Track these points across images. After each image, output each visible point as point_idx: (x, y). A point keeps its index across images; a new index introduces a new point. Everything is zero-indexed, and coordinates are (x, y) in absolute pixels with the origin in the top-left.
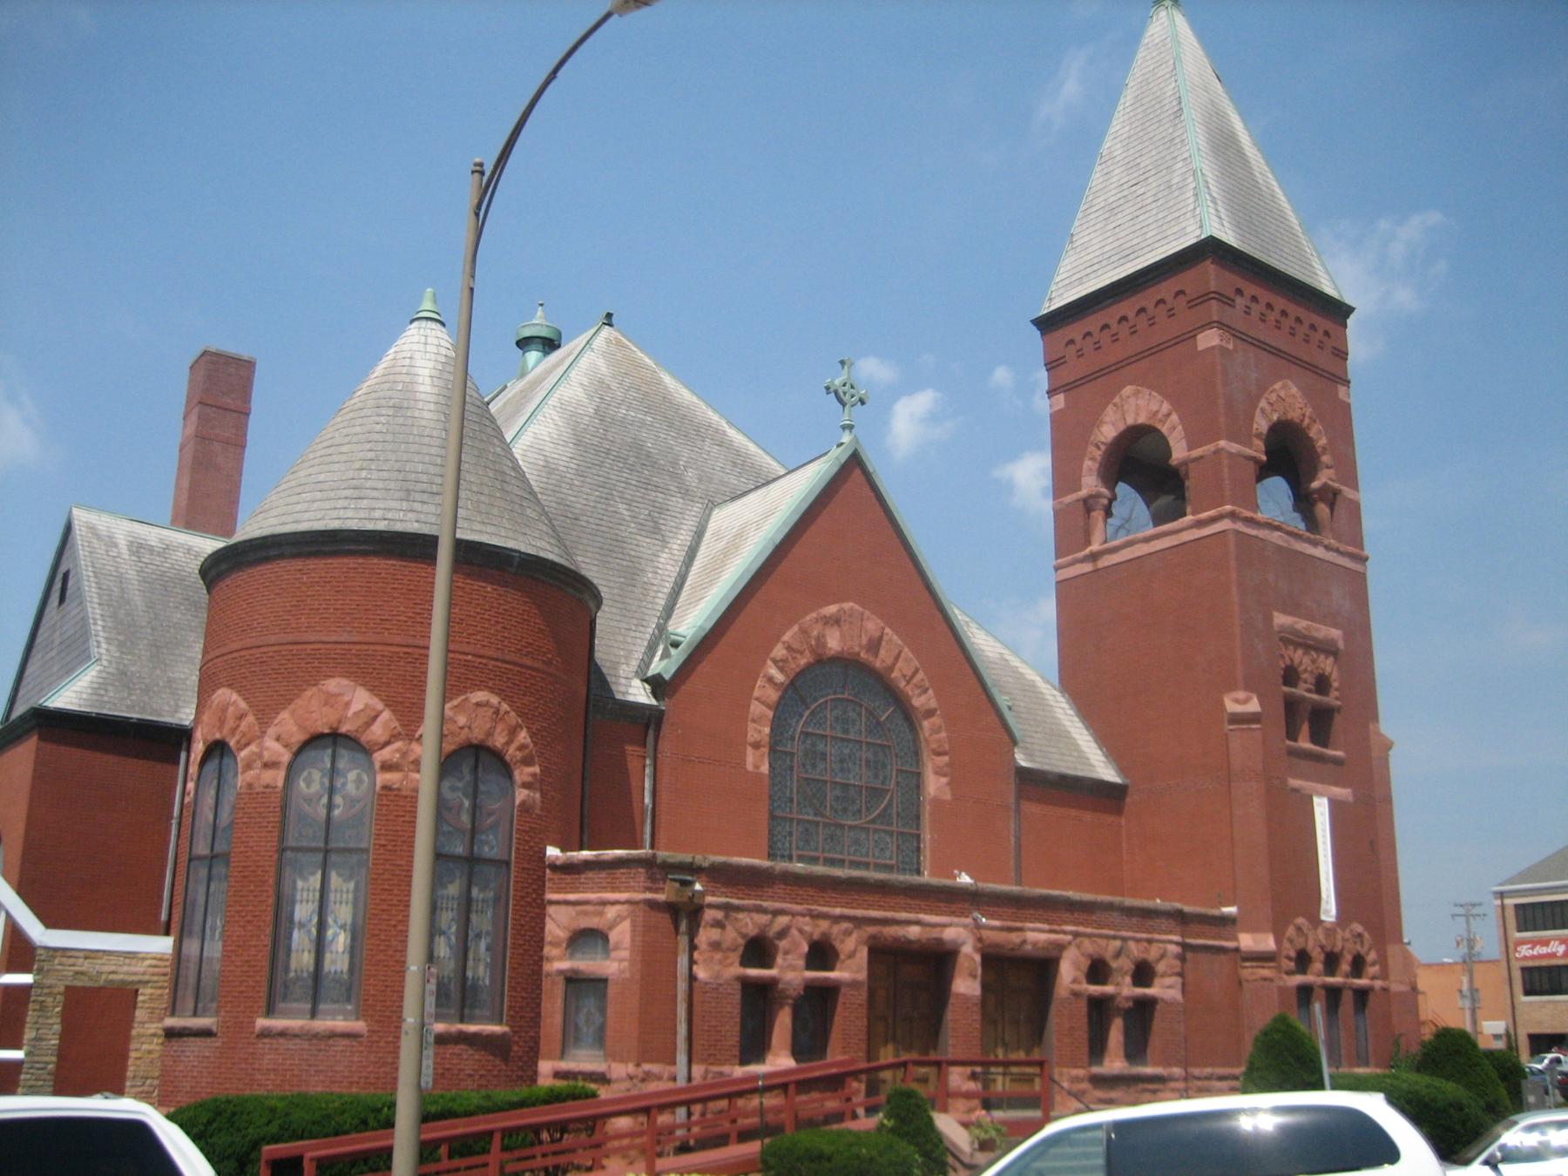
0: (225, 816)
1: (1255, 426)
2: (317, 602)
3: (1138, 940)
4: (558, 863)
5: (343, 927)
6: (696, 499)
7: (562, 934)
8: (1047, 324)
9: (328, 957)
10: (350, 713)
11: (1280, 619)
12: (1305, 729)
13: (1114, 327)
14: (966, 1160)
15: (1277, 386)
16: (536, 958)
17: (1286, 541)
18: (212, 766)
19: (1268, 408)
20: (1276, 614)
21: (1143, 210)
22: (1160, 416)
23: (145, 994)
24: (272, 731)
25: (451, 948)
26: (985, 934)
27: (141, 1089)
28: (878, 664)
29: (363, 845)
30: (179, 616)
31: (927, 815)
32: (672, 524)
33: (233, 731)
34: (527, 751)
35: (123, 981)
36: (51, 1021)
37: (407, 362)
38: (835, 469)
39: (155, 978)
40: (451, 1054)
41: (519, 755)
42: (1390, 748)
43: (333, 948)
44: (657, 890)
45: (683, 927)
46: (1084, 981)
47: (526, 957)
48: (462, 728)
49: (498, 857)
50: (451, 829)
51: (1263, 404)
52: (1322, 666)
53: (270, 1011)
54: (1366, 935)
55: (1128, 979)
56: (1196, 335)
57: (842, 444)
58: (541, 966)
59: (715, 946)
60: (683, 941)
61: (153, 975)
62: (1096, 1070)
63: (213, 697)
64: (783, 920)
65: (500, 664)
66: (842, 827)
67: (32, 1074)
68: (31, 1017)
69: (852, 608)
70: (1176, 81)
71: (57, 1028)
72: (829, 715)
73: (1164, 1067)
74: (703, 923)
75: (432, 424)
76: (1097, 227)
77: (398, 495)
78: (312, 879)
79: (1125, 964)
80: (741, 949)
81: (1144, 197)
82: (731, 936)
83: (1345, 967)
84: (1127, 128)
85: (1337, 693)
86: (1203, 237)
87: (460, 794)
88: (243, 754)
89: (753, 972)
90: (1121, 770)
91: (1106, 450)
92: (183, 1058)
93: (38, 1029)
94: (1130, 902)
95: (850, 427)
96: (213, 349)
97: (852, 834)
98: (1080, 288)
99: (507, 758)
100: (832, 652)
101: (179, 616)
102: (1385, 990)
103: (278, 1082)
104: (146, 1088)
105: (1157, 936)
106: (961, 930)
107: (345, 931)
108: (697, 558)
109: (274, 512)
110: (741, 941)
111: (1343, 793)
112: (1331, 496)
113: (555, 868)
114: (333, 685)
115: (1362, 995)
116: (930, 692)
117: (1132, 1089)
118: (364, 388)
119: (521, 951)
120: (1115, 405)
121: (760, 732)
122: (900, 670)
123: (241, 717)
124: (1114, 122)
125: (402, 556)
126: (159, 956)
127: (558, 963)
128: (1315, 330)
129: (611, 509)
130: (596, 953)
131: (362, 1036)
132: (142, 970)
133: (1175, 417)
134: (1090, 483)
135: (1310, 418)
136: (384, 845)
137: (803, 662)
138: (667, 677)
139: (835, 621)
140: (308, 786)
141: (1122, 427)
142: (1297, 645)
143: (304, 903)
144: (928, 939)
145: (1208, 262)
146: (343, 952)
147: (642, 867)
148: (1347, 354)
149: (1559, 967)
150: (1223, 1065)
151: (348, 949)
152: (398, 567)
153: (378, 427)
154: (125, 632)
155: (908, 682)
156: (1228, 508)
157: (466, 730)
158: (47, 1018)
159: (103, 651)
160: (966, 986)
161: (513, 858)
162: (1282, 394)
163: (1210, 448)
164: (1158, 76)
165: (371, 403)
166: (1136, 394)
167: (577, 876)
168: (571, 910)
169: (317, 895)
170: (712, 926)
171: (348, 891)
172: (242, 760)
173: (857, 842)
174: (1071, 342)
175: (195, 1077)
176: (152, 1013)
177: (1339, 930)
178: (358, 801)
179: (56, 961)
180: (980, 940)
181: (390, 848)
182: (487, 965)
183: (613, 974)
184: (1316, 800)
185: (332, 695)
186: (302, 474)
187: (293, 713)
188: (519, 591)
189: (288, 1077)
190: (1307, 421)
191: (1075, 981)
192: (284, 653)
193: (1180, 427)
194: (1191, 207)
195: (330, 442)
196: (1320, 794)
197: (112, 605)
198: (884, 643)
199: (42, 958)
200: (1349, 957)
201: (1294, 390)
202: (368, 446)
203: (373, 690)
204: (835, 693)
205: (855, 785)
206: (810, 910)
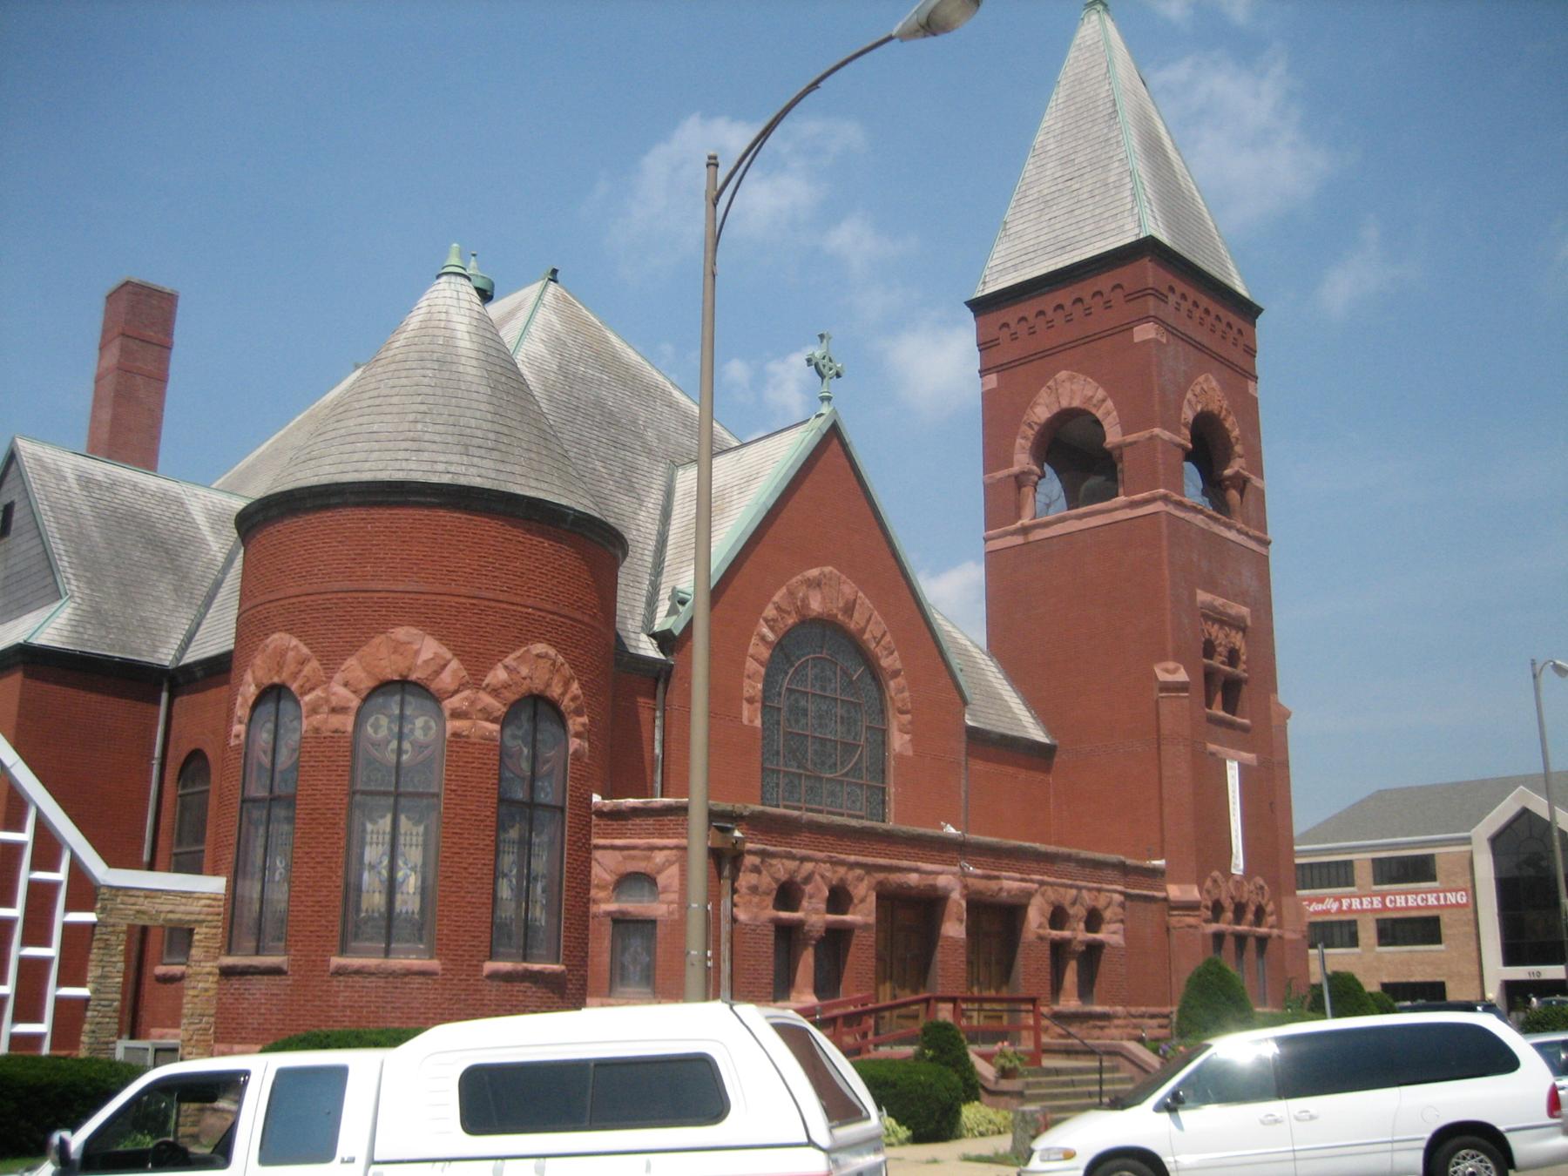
0: (284, 759)
1: (1183, 416)
3: (1090, 889)
4: (605, 809)
5: (413, 869)
6: (659, 459)
7: (609, 878)
8: (980, 306)
9: (399, 897)
11: (1203, 596)
12: (1219, 697)
13: (1050, 313)
14: (991, 1086)
15: (1201, 379)
16: (585, 900)
17: (1207, 524)
18: (268, 708)
19: (1193, 399)
20: (1199, 592)
21: (1079, 205)
22: (1095, 401)
23: (200, 933)
24: (338, 676)
25: (512, 890)
26: (970, 881)
27: (198, 1026)
28: (852, 626)
29: (434, 790)
30: (138, 554)
31: (892, 770)
32: (644, 483)
33: (295, 675)
34: (579, 702)
35: (180, 920)
36: (114, 959)
37: (443, 316)
38: (818, 439)
39: (210, 918)
40: (518, 991)
41: (572, 705)
42: (1288, 718)
43: (404, 889)
45: (726, 872)
46: (1048, 926)
47: (578, 899)
48: (524, 678)
49: (553, 803)
50: (512, 775)
51: (1189, 395)
52: (1233, 640)
53: (343, 951)
54: (1266, 887)
55: (1082, 925)
56: (1132, 328)
57: (821, 415)
58: (588, 908)
59: (754, 890)
60: (726, 884)
61: (208, 914)
62: (1056, 1008)
63: (268, 641)
64: (809, 866)
65: (555, 617)
66: (821, 779)
67: (99, 1011)
68: (95, 954)
69: (831, 572)
70: (1110, 84)
71: (121, 966)
72: (810, 673)
73: (1110, 1006)
74: (743, 869)
75: (476, 380)
76: (1032, 216)
77: (456, 449)
78: (381, 822)
79: (1078, 911)
80: (774, 893)
81: (1081, 192)
82: (765, 881)
83: (1250, 916)
84: (1060, 125)
85: (1244, 667)
86: (1142, 236)
87: (520, 742)
88: (307, 698)
89: (784, 915)
90: (1049, 731)
91: (1039, 430)
92: (247, 996)
93: (103, 967)
94: (1084, 854)
95: (829, 399)
96: (135, 279)
97: (828, 786)
99: (562, 708)
100: (815, 614)
101: (138, 554)
102: (1280, 937)
103: (355, 1018)
104: (202, 1026)
105: (1105, 886)
106: (950, 877)
107: (415, 873)
108: (673, 517)
109: (328, 460)
110: (775, 886)
111: (1249, 757)
112: (1241, 483)
113: (601, 814)
114: (401, 633)
115: (1262, 941)
116: (896, 653)
117: (1085, 1026)
118: (401, 340)
119: (574, 893)
120: (1049, 388)
121: (754, 688)
122: (871, 631)
123: (303, 662)
124: (1047, 117)
125: (467, 509)
126: (213, 896)
127: (606, 905)
128: (1231, 328)
129: (590, 466)
130: (643, 896)
131: (436, 974)
132: (198, 909)
133: (1109, 403)
134: (1022, 460)
135: (1226, 410)
136: (454, 791)
137: (790, 621)
138: (677, 632)
139: (816, 584)
140: (376, 732)
141: (1055, 409)
142: (1215, 621)
143: (374, 846)
144: (925, 886)
145: (1147, 260)
146: (414, 893)
148: (1255, 352)
149: (1332, 923)
150: (1154, 1005)
151: (419, 890)
152: (463, 520)
153: (426, 381)
154: (91, 569)
155: (878, 643)
156: (1162, 491)
157: (528, 681)
158: (112, 956)
159: (74, 588)
160: (954, 929)
162: (1205, 387)
163: (1145, 434)
164: (1091, 76)
165: (415, 356)
166: (1071, 379)
167: (624, 823)
169: (387, 838)
170: (752, 871)
171: (417, 834)
172: (306, 704)
173: (832, 794)
174: (1006, 325)
175: (264, 1014)
176: (207, 952)
177: (1245, 883)
178: (427, 747)
179: (119, 900)
180: (966, 887)
181: (459, 793)
182: (543, 906)
183: (662, 916)
184: (1229, 763)
185: (402, 644)
186: (351, 423)
187: (360, 660)
188: (572, 547)
189: (364, 1013)
190: (1224, 413)
191: (1040, 926)
193: (1115, 413)
194: (1129, 206)
195: (375, 393)
196: (1233, 759)
197: (73, 541)
198: (857, 606)
199: (106, 896)
200: (1252, 908)
201: (1214, 384)
202: (419, 399)
203: (441, 639)
204: (815, 653)
205: (830, 740)
206: (831, 857)
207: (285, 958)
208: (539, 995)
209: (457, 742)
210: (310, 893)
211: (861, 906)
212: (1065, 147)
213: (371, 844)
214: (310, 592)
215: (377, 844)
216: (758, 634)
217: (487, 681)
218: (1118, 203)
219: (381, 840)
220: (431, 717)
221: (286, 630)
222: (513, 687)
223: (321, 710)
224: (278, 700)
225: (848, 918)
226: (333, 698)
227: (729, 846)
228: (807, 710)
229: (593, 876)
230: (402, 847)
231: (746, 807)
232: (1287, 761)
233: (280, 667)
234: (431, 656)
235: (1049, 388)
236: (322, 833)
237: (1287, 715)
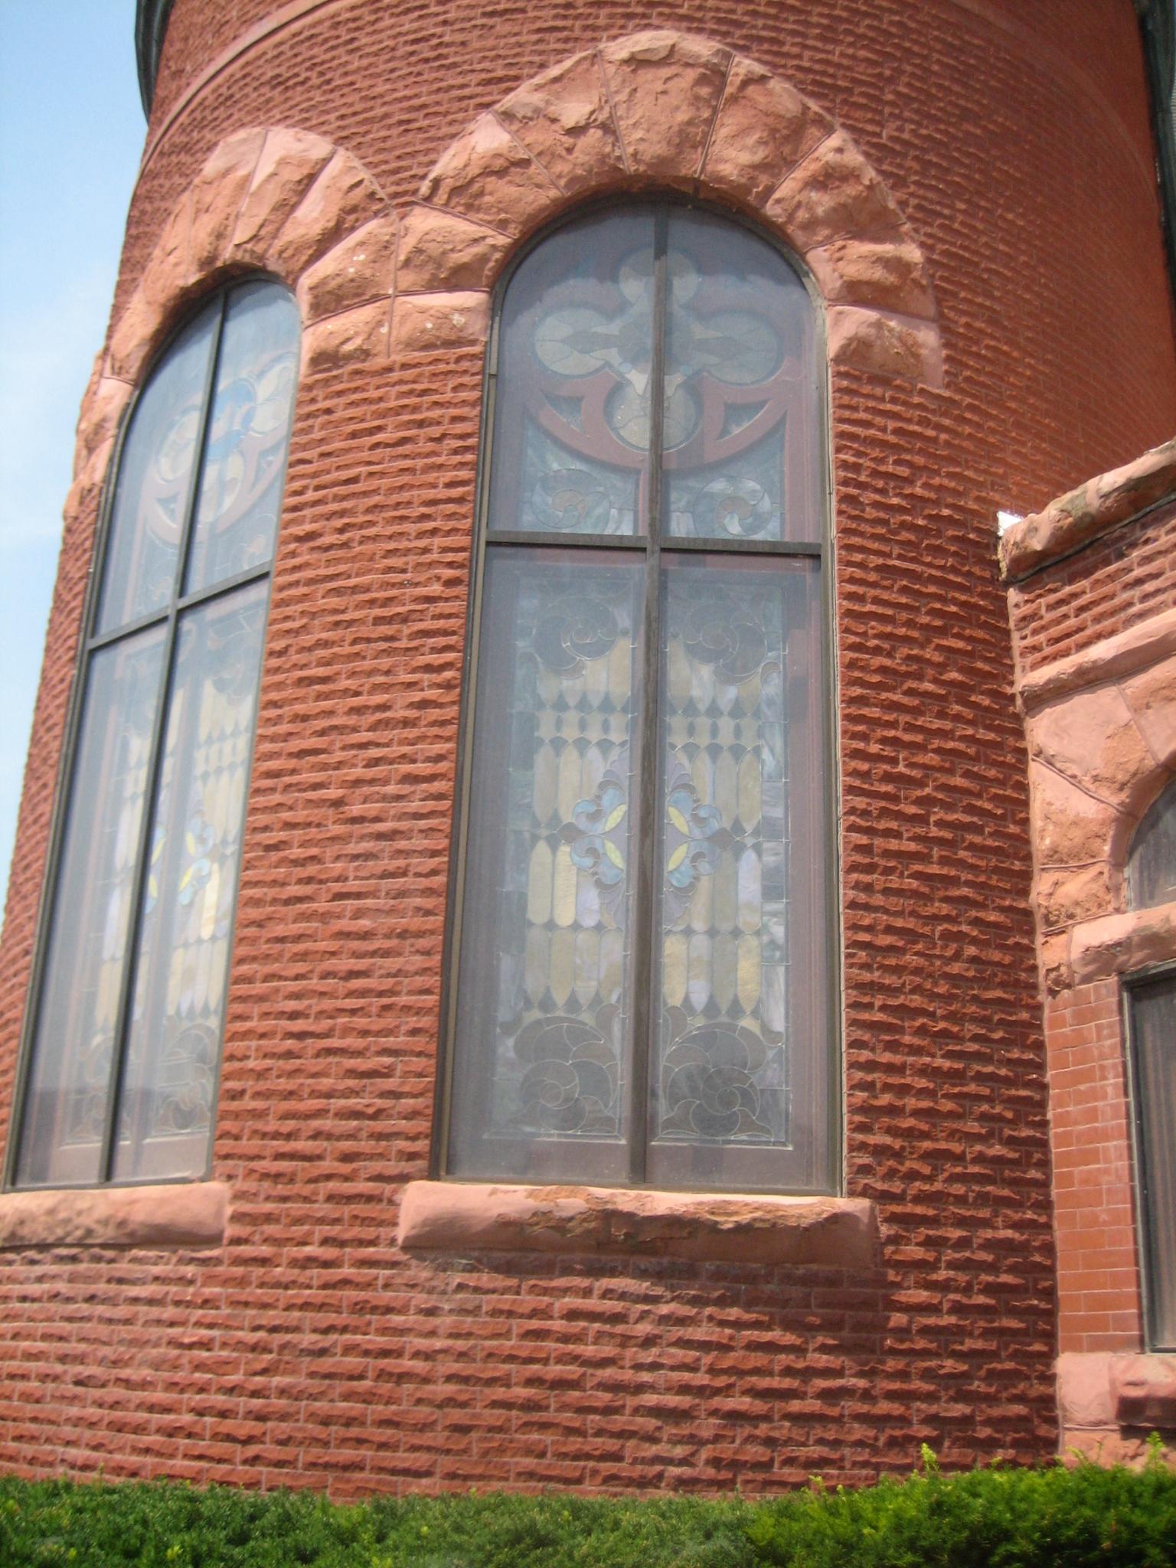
34: (851, 190)
41: (823, 202)
48: (575, 131)
146: (214, 938)
157: (595, 134)
161: (833, 532)
168: (1108, 700)
229: (1037, 822)
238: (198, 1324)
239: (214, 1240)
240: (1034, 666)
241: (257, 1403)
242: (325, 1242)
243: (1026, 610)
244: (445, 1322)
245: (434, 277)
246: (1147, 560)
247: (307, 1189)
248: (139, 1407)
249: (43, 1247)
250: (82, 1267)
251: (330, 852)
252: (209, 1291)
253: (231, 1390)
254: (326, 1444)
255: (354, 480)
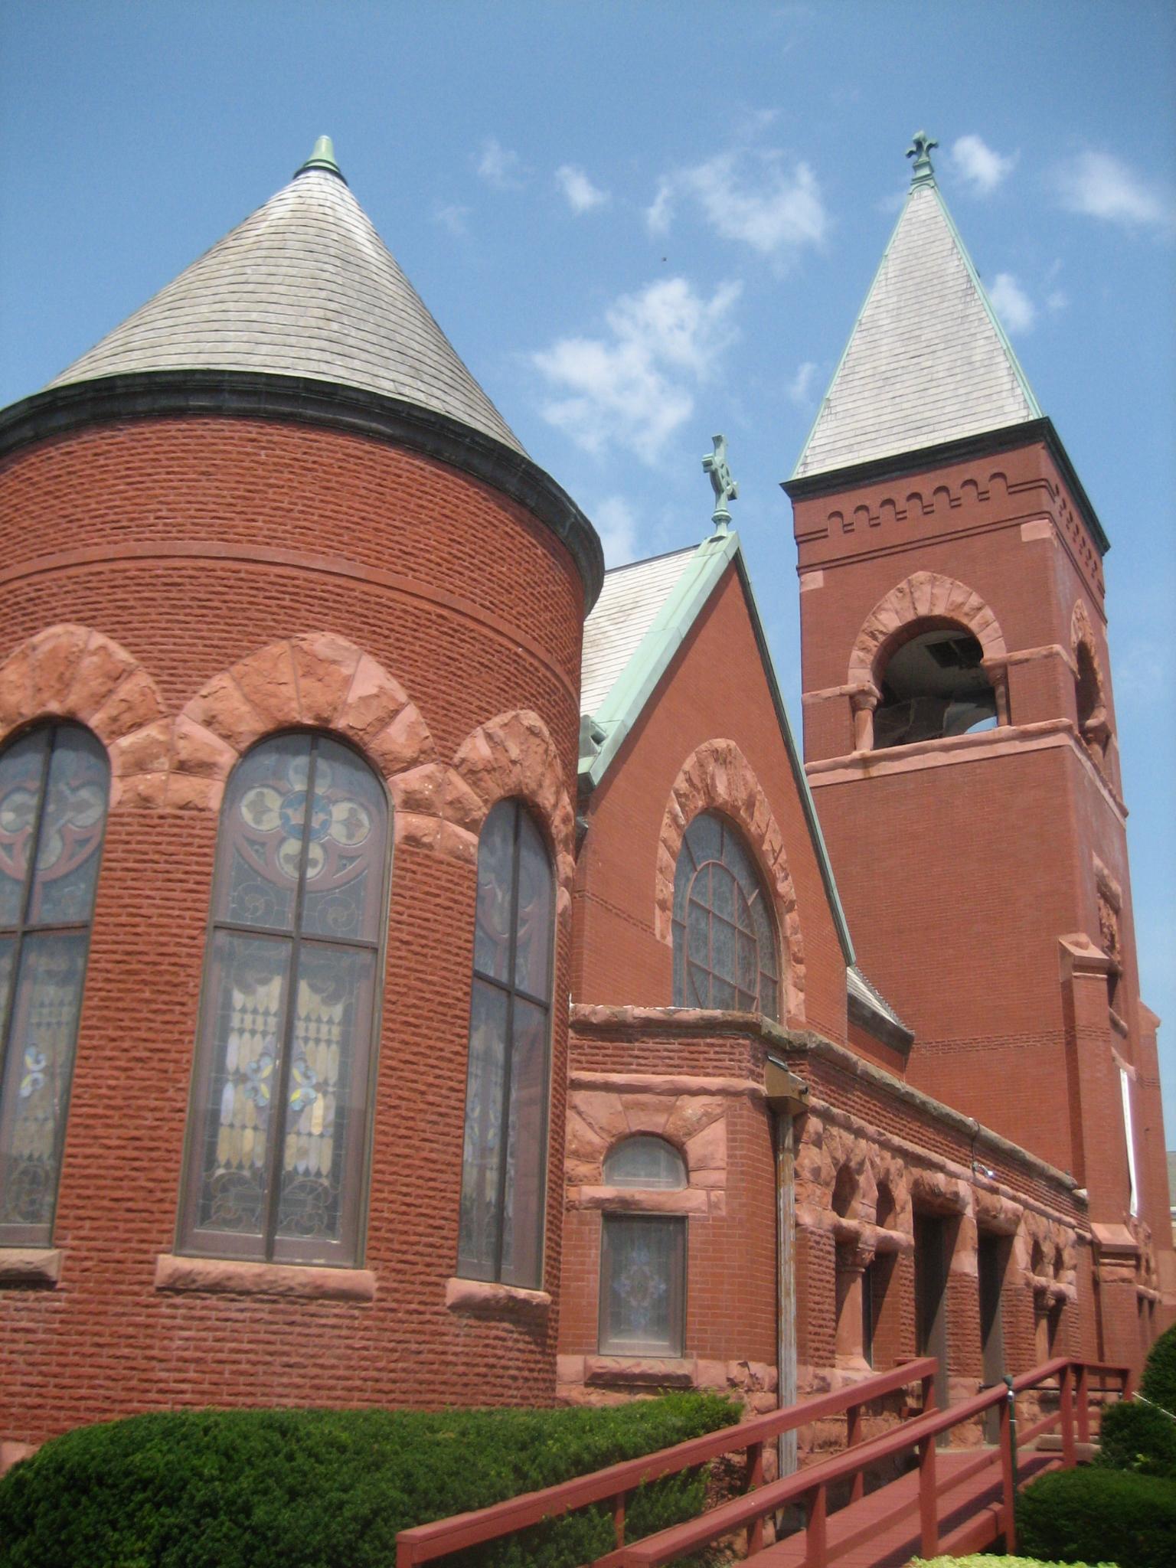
2: (287, 499)
5: (321, 1087)
8: (801, 490)
9: (291, 1140)
10: (352, 697)
21: (934, 383)
22: (966, 609)
24: (194, 706)
29: (368, 938)
43: (302, 1125)
44: (757, 1077)
45: (789, 1141)
48: (514, 762)
53: (180, 1246)
56: (1018, 525)
57: (721, 538)
59: (816, 1172)
63: (37, 639)
74: (805, 1137)
78: (261, 990)
80: (833, 1183)
81: (934, 370)
84: (895, 299)
88: (125, 742)
98: (850, 456)
100: (720, 800)
107: (325, 1094)
114: (322, 642)
120: (901, 591)
123: (118, 676)
130: (657, 1175)
131: (369, 1299)
133: (988, 613)
136: (407, 943)
139: (721, 758)
140: (258, 821)
141: (910, 617)
143: (247, 1036)
146: (322, 1136)
147: (744, 1038)
151: (331, 1130)
155: (776, 859)
161: (554, 1000)
163: (1042, 650)
166: (933, 581)
171: (330, 1022)
172: (123, 753)
178: (352, 859)
180: (977, 1201)
186: (204, 309)
187: (238, 681)
192: (220, 573)
193: (996, 624)
194: (1008, 386)
198: (757, 804)
206: (881, 1134)
207: (54, 1252)
208: (521, 1346)
209: (412, 854)
210: (116, 1121)
211: (902, 1216)
212: (904, 323)
213: (241, 1031)
214: (139, 553)
215: (253, 1032)
216: (670, 812)
217: (462, 753)
218: (993, 383)
219: (260, 1027)
220: (362, 805)
221: (80, 620)
222: (497, 774)
223: (156, 765)
224: (52, 746)
225: (894, 1234)
226: (181, 743)
227: (796, 1096)
228: (706, 937)
229: (568, 1137)
230: (301, 1042)
231: (811, 1035)
232: (1158, 1080)
233: (65, 684)
234: (375, 691)
235: (901, 591)
236: (148, 1001)
237: (1157, 1024)
238: (362, 1338)
239: (369, 1299)
240: (577, 1069)
241: (392, 1375)
242: (420, 1303)
243: (575, 1042)
244: (461, 1340)
245: (462, 819)
246: (643, 1050)
247: (412, 1278)
248: (331, 1378)
249: (247, 1293)
250: (281, 1306)
251: (419, 1116)
252: (367, 1323)
253: (379, 1370)
254: (420, 1392)
255: (427, 920)
